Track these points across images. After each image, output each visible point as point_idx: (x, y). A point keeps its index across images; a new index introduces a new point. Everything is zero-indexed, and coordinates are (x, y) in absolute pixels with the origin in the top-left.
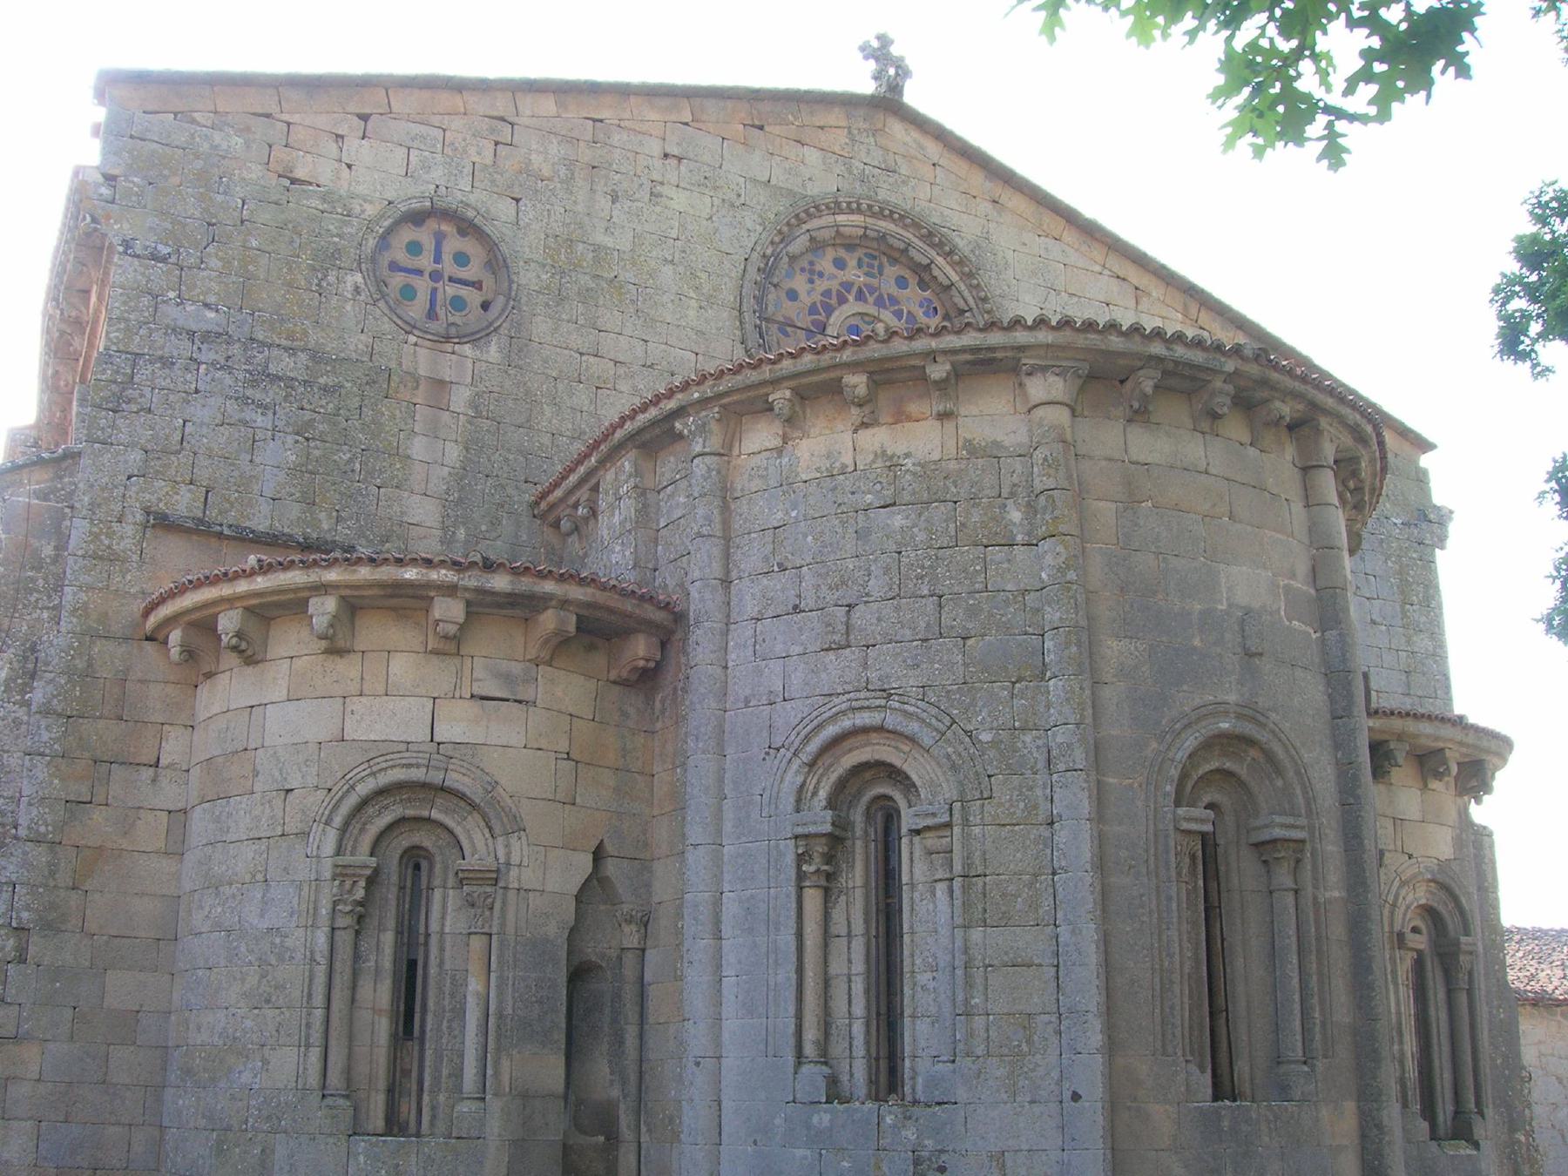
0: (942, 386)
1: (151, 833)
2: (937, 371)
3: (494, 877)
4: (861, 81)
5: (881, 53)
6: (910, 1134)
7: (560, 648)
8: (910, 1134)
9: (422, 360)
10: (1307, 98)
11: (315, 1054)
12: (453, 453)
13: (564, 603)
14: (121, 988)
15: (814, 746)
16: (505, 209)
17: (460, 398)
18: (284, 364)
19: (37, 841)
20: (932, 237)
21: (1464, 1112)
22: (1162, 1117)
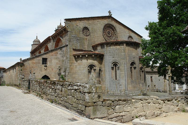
0: (119, 44)
1: (75, 67)
2: (119, 43)
3: (95, 69)
4: (108, 15)
5: (110, 12)
6: (118, 82)
7: (98, 57)
8: (118, 82)
9: (85, 37)
10: (146, 55)
11: (87, 79)
12: (87, 43)
13: (99, 55)
14: (74, 76)
15: (112, 62)
16: (89, 26)
17: (88, 40)
18: (78, 38)
19: (69, 68)
20: (113, 26)
21: (25, 69)
22: (130, 81)
